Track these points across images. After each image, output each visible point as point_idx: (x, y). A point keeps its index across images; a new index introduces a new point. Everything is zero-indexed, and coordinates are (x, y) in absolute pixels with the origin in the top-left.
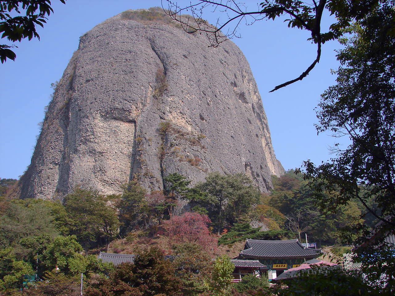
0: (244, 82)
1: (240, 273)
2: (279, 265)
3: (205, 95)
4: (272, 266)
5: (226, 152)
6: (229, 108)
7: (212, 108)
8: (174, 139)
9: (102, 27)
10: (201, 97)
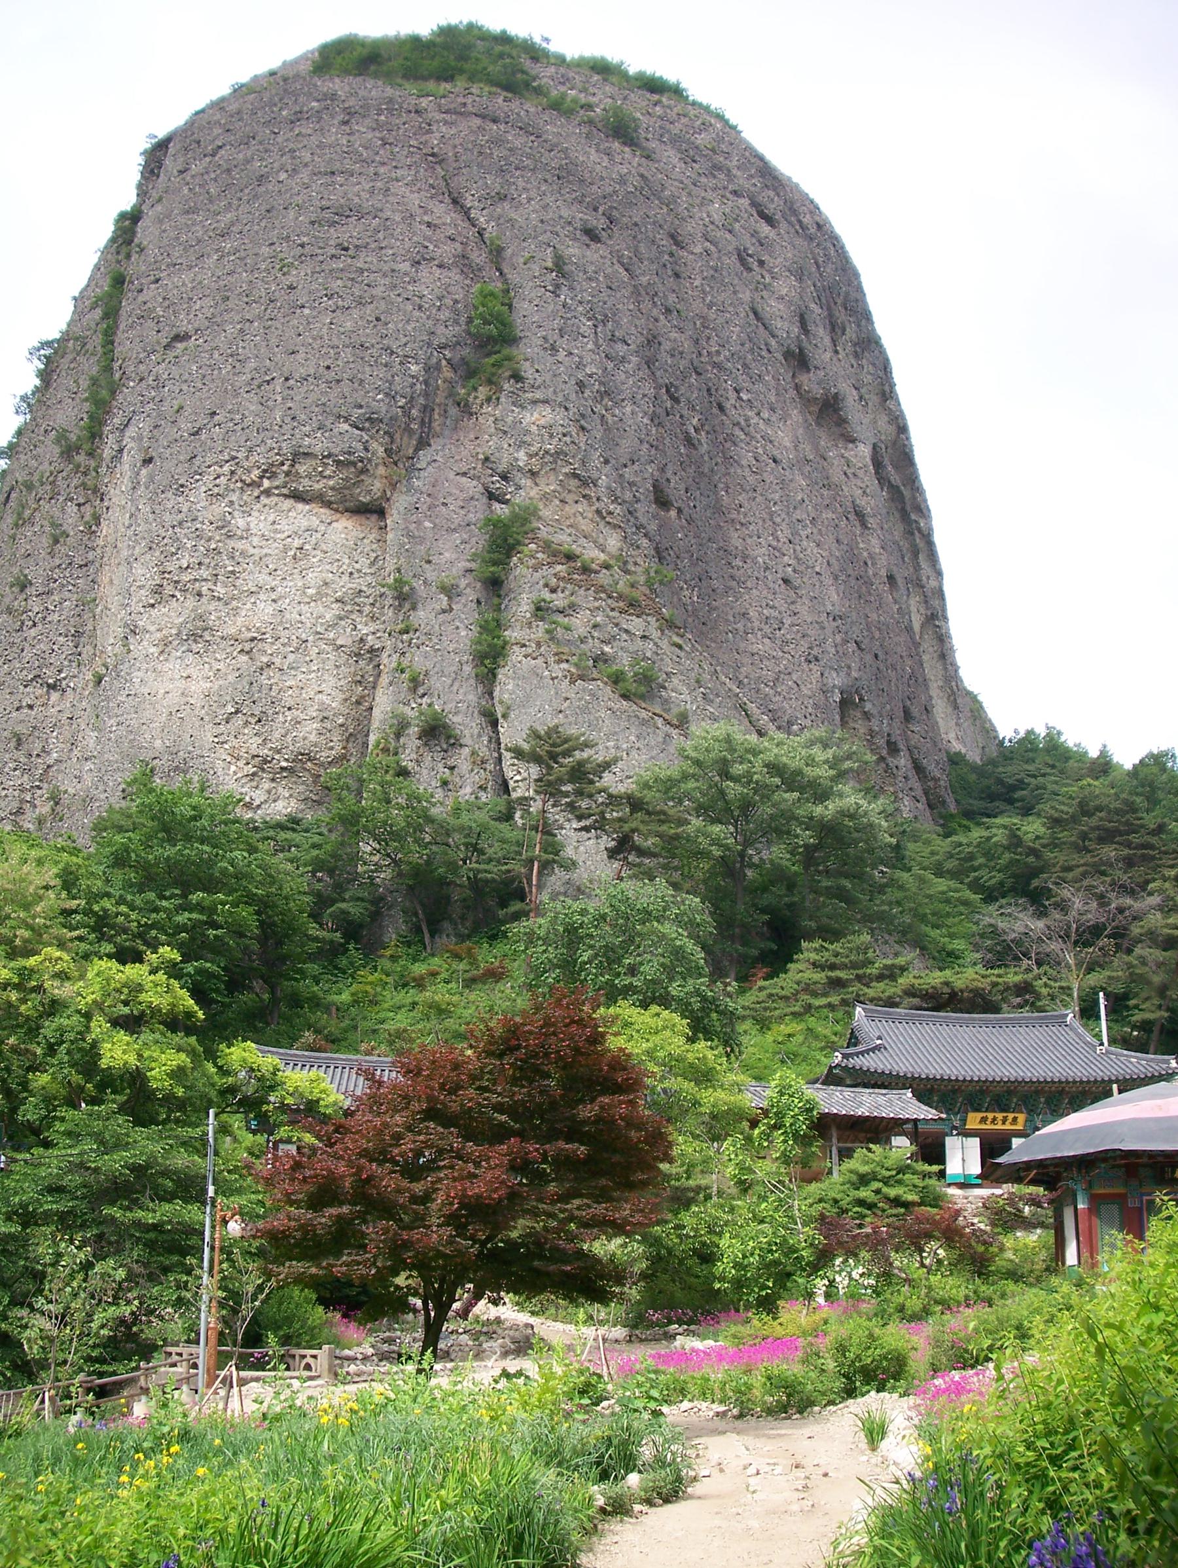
0: (836, 352)
1: (834, 1140)
2: (990, 1116)
3: (676, 400)
4: (964, 1121)
5: (761, 646)
6: (775, 461)
7: (706, 458)
8: (546, 585)
9: (233, 107)
10: (659, 410)
